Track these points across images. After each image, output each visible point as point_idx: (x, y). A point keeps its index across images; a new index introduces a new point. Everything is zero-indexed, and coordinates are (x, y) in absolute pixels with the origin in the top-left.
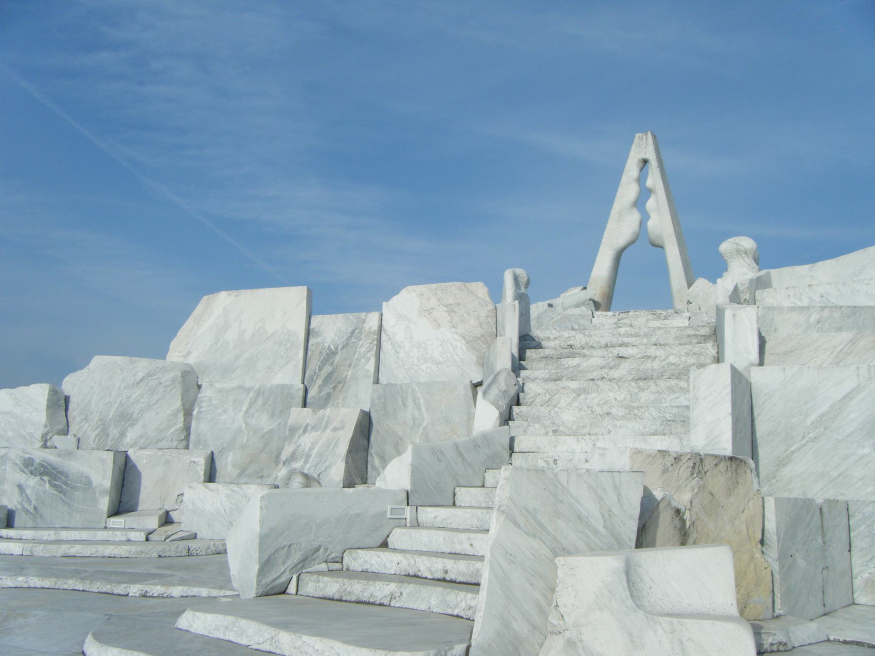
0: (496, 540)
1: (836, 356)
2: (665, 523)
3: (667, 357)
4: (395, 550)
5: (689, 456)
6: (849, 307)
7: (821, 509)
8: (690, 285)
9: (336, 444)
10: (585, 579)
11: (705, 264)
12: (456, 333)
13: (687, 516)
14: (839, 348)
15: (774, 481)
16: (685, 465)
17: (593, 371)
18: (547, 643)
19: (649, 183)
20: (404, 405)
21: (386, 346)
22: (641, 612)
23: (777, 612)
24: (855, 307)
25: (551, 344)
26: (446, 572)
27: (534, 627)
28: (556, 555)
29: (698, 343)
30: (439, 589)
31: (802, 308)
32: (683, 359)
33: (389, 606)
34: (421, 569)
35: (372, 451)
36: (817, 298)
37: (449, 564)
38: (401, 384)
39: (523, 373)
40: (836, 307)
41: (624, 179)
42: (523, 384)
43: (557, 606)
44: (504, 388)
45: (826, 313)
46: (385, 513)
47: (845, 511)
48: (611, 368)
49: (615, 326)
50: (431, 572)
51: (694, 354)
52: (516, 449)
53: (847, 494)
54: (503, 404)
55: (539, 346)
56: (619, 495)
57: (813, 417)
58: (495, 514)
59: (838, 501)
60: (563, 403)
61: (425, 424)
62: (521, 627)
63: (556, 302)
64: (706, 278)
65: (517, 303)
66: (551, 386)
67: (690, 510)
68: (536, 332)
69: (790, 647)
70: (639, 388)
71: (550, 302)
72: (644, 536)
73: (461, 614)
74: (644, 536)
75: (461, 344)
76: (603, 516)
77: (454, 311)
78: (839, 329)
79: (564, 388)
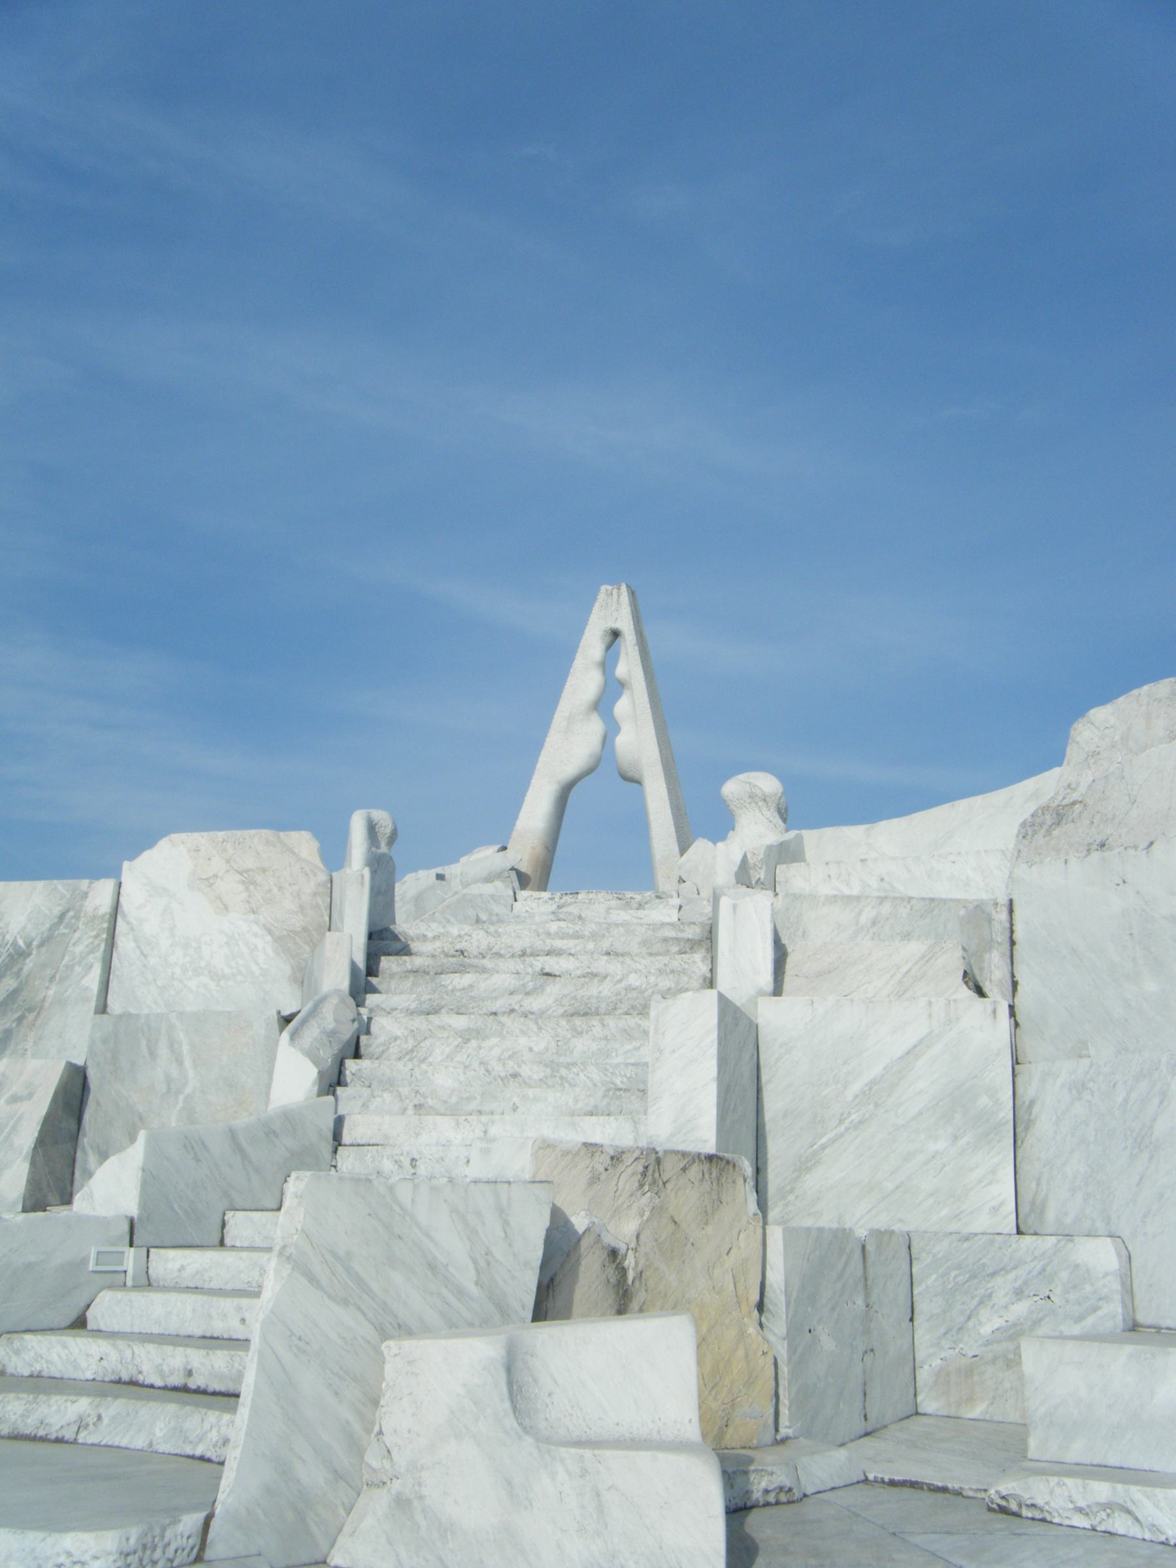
0: (272, 1311)
1: (900, 982)
2: (590, 1275)
3: (625, 977)
4: (99, 1333)
5: (637, 1154)
6: (923, 899)
7: (863, 1247)
8: (683, 850)
9: (14, 1128)
10: (439, 1378)
11: (703, 819)
12: (256, 922)
13: (630, 1262)
14: (904, 969)
15: (791, 1197)
16: (630, 1170)
17: (496, 998)
18: (362, 1501)
19: (621, 671)
20: (151, 1053)
21: (124, 943)
22: (529, 1440)
23: (784, 1432)
24: (932, 900)
25: (427, 947)
26: (190, 1373)
27: (338, 1475)
28: (385, 1336)
29: (680, 953)
30: (172, 1407)
31: (849, 899)
32: (652, 979)
33: (75, 1442)
34: (145, 1368)
35: (85, 1141)
36: (874, 882)
37: (196, 1358)
38: (148, 1016)
39: (371, 999)
40: (902, 899)
41: (579, 662)
42: (370, 1019)
43: (381, 1432)
44: (330, 1024)
45: (886, 908)
46: (84, 1261)
47: (904, 1249)
48: (528, 994)
49: (551, 917)
50: (161, 1374)
51: (672, 971)
52: (346, 1138)
53: (911, 1221)
54: (328, 1055)
55: (405, 951)
56: (506, 1223)
57: (856, 1087)
58: (272, 1262)
59: (893, 1232)
60: (438, 1054)
61: (188, 1090)
62: (312, 1475)
63: (446, 870)
64: (704, 837)
65: (367, 872)
66: (419, 1022)
67: (635, 1250)
68: (404, 924)
69: (797, 1494)
70: (574, 1029)
71: (439, 870)
72: (549, 1301)
73: (208, 1455)
74: (549, 1301)
75: (264, 944)
76: (475, 1262)
77: (254, 883)
78: (907, 936)
79: (443, 1028)
